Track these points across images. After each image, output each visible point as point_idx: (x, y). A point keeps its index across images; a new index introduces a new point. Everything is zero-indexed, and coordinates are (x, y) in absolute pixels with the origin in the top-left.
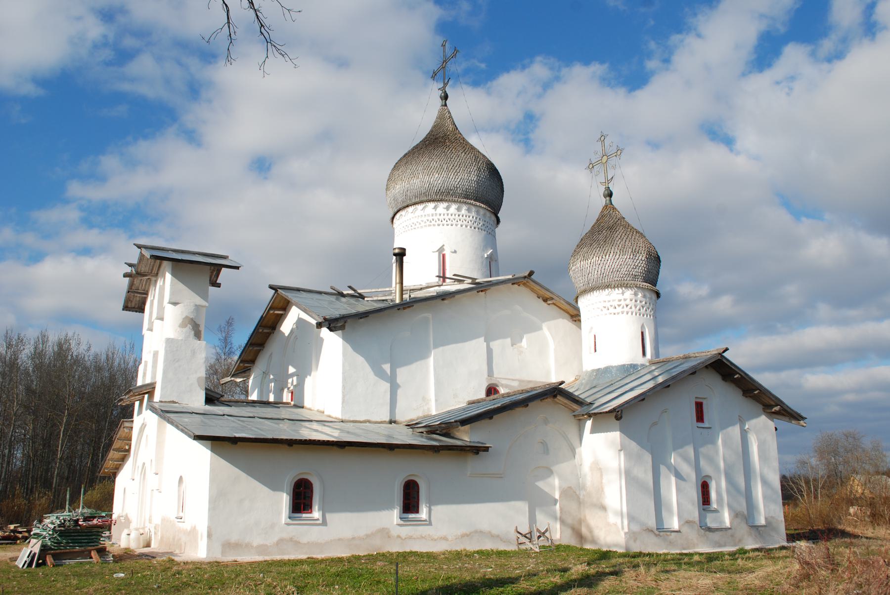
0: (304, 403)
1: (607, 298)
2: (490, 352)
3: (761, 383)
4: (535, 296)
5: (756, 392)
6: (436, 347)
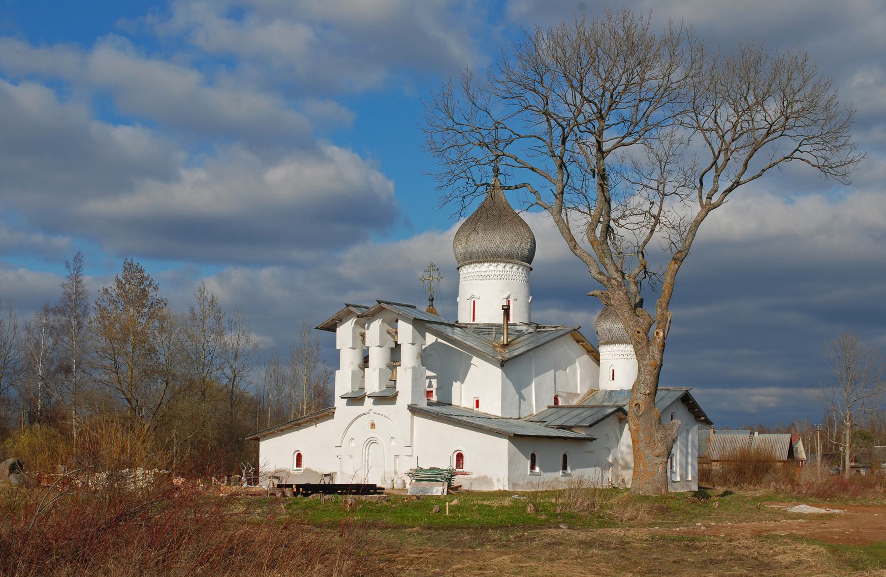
0: (451, 401)
1: (624, 349)
2: (555, 374)
3: (702, 408)
4: (573, 338)
5: (696, 410)
6: (535, 377)
